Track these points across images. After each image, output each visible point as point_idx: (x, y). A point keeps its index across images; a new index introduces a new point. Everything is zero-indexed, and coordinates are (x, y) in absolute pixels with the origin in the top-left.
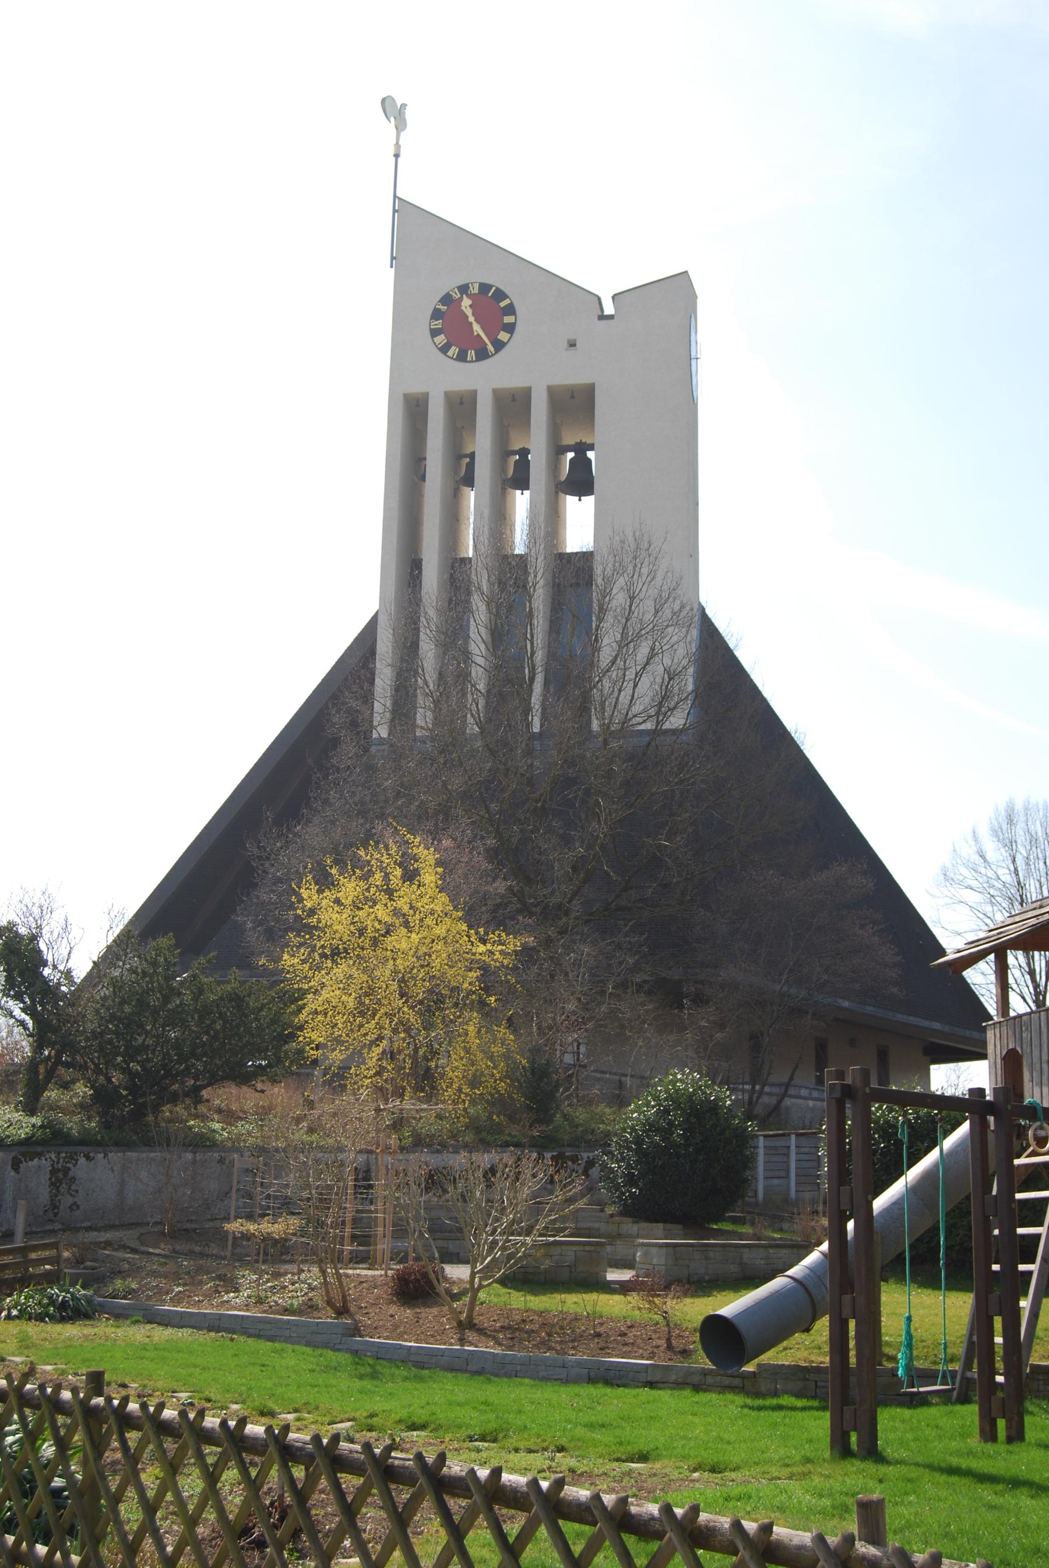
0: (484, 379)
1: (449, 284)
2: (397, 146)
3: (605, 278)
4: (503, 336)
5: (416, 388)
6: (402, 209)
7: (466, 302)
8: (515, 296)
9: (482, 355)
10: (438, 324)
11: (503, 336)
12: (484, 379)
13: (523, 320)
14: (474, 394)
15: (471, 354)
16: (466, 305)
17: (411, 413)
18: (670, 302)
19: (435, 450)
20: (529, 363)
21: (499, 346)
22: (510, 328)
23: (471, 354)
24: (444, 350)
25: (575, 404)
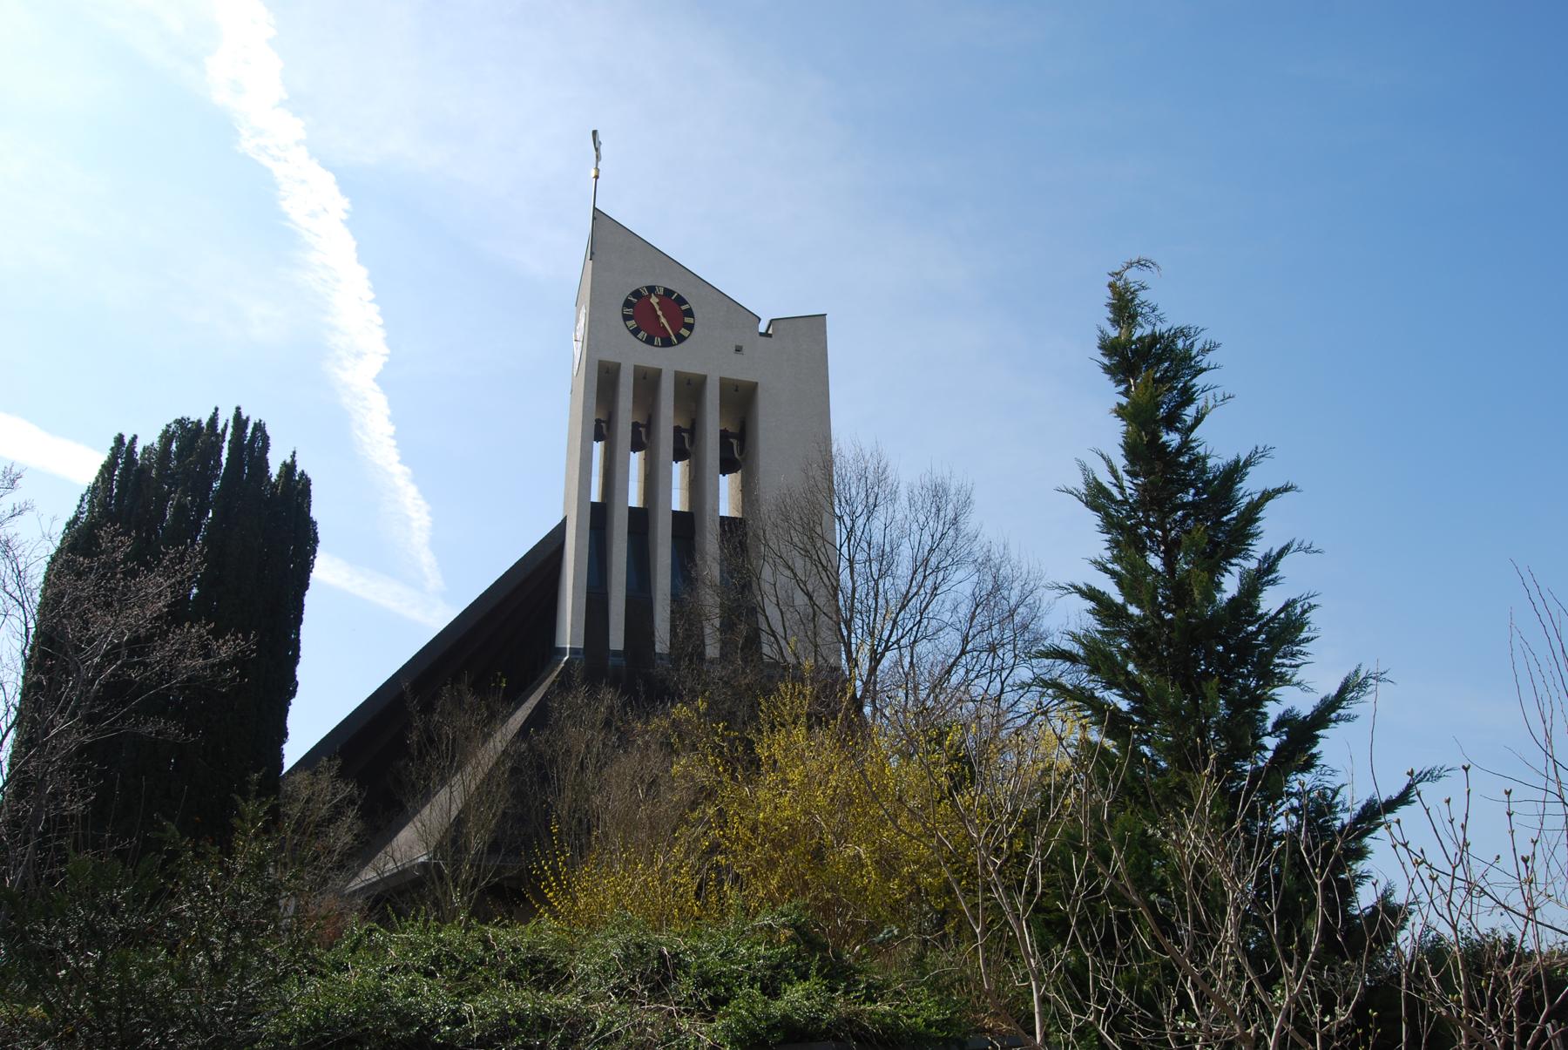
0: (669, 361)
1: (641, 283)
2: (597, 170)
3: (767, 304)
4: (684, 332)
5: (610, 356)
6: (598, 215)
7: (654, 300)
8: (693, 303)
9: (667, 343)
10: (629, 311)
11: (684, 332)
12: (669, 361)
13: (699, 319)
14: (658, 373)
15: (658, 340)
16: (649, 304)
17: (604, 380)
18: (808, 331)
19: (617, 407)
20: (700, 355)
21: (681, 339)
22: (690, 327)
23: (658, 340)
24: (635, 332)
25: (741, 399)
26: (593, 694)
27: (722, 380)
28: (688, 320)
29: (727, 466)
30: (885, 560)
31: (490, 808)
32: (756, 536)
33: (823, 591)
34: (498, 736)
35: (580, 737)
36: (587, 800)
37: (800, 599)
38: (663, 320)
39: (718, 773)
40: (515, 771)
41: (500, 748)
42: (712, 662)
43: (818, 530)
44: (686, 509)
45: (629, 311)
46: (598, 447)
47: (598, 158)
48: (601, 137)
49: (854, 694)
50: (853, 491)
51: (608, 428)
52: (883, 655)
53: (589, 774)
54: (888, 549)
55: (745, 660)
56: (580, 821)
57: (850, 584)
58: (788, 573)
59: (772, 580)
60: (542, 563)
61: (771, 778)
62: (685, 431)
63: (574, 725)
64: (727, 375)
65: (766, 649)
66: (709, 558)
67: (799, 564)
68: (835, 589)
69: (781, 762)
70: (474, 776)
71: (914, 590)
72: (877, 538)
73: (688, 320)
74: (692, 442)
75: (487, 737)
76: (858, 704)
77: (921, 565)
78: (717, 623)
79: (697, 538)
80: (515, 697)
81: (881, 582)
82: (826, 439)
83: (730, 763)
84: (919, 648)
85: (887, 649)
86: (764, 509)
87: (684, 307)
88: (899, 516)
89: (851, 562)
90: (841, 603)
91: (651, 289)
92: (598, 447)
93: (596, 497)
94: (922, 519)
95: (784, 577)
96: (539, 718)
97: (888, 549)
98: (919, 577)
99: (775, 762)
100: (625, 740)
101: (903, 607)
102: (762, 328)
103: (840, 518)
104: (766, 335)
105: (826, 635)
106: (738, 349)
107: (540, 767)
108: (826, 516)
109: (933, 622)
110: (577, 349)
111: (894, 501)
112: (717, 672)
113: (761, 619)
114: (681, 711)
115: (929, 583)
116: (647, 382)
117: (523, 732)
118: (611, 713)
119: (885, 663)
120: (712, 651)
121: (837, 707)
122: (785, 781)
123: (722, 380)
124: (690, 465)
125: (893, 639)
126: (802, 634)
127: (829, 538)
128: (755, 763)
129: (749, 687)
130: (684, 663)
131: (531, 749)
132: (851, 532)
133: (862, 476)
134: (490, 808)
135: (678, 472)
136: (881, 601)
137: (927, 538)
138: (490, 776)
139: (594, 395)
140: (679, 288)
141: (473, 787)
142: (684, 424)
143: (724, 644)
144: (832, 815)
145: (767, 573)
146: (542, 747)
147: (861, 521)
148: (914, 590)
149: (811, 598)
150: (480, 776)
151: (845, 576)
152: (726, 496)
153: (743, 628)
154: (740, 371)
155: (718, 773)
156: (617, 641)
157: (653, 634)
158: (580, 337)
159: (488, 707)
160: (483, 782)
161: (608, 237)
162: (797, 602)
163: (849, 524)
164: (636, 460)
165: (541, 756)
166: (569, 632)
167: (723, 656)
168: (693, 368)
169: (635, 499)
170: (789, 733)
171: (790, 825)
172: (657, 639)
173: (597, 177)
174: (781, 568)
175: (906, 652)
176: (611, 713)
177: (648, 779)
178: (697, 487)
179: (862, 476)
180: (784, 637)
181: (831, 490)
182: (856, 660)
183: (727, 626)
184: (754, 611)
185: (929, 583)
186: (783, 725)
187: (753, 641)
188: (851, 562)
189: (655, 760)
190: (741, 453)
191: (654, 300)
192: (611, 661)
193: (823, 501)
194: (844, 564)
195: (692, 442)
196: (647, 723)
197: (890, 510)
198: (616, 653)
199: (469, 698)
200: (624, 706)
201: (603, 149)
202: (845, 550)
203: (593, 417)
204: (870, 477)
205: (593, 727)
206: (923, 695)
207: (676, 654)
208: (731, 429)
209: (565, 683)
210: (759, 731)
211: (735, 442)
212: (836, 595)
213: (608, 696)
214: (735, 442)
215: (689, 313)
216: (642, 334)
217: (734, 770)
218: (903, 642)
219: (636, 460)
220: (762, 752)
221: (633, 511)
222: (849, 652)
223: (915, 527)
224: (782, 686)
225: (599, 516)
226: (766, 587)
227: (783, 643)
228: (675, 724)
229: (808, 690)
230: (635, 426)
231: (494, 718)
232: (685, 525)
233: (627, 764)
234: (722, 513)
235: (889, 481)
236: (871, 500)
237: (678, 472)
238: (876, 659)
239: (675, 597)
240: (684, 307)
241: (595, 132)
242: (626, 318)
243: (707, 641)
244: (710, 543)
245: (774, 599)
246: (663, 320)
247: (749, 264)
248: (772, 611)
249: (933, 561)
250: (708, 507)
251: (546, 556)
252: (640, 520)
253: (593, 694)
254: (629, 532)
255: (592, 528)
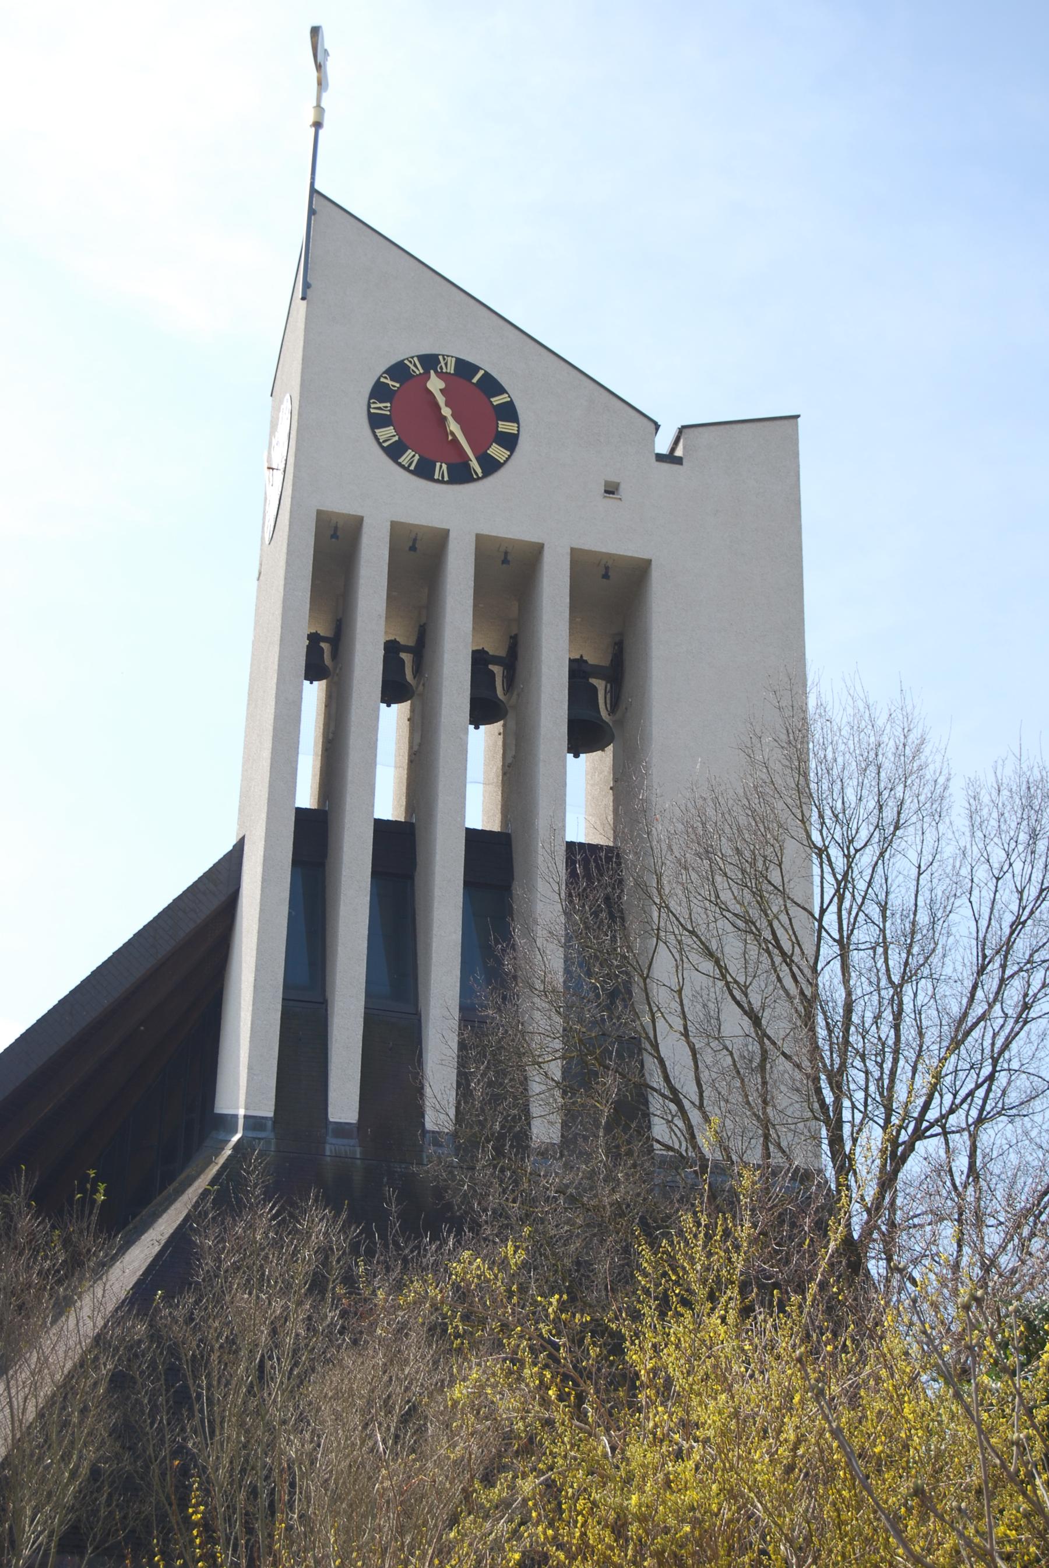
0: (465, 515)
2: (319, 109)
3: (673, 397)
4: (497, 451)
5: (341, 504)
6: (318, 202)
7: (435, 384)
8: (516, 391)
9: (461, 475)
10: (383, 408)
11: (497, 451)
12: (465, 515)
15: (441, 469)
17: (331, 552)
19: (356, 614)
21: (491, 466)
22: (510, 442)
23: (441, 469)
24: (394, 452)
25: (614, 593)
26: (287, 1220)
27: (481, 540)
28: (505, 427)
29: (584, 736)
30: (914, 948)
31: (66, 1458)
32: (641, 886)
33: (783, 1008)
34: (86, 1305)
35: (259, 1308)
36: (271, 1445)
37: (734, 1024)
38: (454, 427)
39: (545, 1402)
40: (119, 1381)
41: (89, 1329)
42: (544, 1153)
43: (775, 876)
44: (495, 827)
45: (383, 408)
46: (313, 694)
47: (321, 84)
48: (328, 41)
49: (850, 1234)
50: (851, 795)
51: (335, 654)
52: (910, 1147)
53: (275, 1392)
54: (923, 918)
55: (615, 1154)
56: (254, 1492)
57: (840, 995)
58: (708, 966)
59: (675, 984)
60: (192, 937)
61: (659, 1417)
62: (496, 660)
63: (247, 1286)
64: (487, 530)
65: (659, 1130)
66: (541, 933)
67: (732, 948)
68: (810, 1003)
69: (680, 1383)
70: (35, 1387)
71: (978, 1010)
72: (900, 897)
73: (505, 427)
74: (510, 682)
75: (63, 1306)
76: (853, 1253)
77: (993, 955)
78: (555, 1070)
79: (517, 890)
80: (124, 1221)
81: (908, 990)
82: (793, 680)
83: (572, 1381)
84: (988, 1136)
85: (919, 1134)
86: (660, 830)
87: (497, 400)
88: (949, 850)
89: (844, 946)
90: (822, 1032)
91: (430, 362)
92: (313, 694)
93: (306, 797)
94: (998, 856)
95: (699, 978)
96: (172, 1268)
97: (923, 918)
98: (991, 982)
99: (669, 1381)
100: (356, 1318)
101: (956, 1044)
102: (662, 444)
103: (822, 852)
104: (670, 458)
105: (788, 1102)
106: (611, 490)
107: (173, 1372)
108: (791, 848)
109: (1022, 1082)
110: (273, 486)
111: (938, 816)
112: (554, 1176)
113: (651, 1063)
114: (468, 1265)
115: (1013, 994)
116: (418, 559)
117: (141, 1295)
118: (325, 1263)
119: (914, 1167)
120: (545, 1128)
121: (811, 1263)
122: (687, 1426)
123: (481, 540)
124: (505, 734)
125: (932, 1115)
126: (736, 1098)
127: (796, 892)
128: (629, 1380)
129: (620, 1210)
130: (484, 1157)
131: (155, 1336)
132: (844, 882)
133: (871, 763)
134: (66, 1458)
135: (481, 747)
136: (908, 1032)
137: (1008, 898)
138: (67, 1389)
139: (306, 584)
140: (487, 361)
141: (31, 1415)
142: (494, 647)
143: (570, 1116)
144: (786, 1501)
145: (663, 966)
146: (178, 1332)
147: (865, 860)
148: (978, 1010)
149: (756, 1021)
150: (47, 1390)
151: (830, 977)
152: (580, 800)
153: (610, 1083)
154: (614, 536)
155: (545, 1402)
156: (344, 1103)
157: (420, 1091)
158: (278, 462)
159: (66, 1242)
160: (51, 1401)
161: (337, 248)
162: (727, 1030)
163: (840, 863)
164: (392, 722)
165: (174, 1351)
166: (245, 1081)
167: (567, 1142)
168: (514, 527)
169: (387, 802)
170: (698, 1324)
171: (696, 1523)
172: (429, 1102)
173: (318, 125)
174: (694, 957)
175: (960, 1142)
176: (325, 1263)
177: (399, 1408)
178: (517, 777)
179: (871, 763)
180: (698, 1102)
181: (803, 792)
182: (850, 1158)
183: (578, 1078)
184: (636, 1046)
185: (1013, 994)
186: (686, 1303)
187: (632, 1111)
188: (844, 946)
189: (417, 1357)
190: (612, 711)
191: (435, 384)
192: (332, 1146)
193: (784, 815)
194: (829, 950)
195: (510, 682)
196: (399, 1287)
197: (930, 837)
198: (342, 1129)
199: (26, 1223)
200: (355, 1248)
201: (331, 67)
202: (830, 919)
203: (303, 629)
204: (888, 765)
205: (287, 1289)
206: (993, 1237)
207: (468, 1136)
208: (592, 658)
209: (227, 1197)
210: (636, 1316)
211: (600, 684)
212: (809, 1021)
213: (319, 1226)
214: (600, 684)
215: (509, 412)
216: (409, 457)
217: (581, 1398)
218: (953, 1120)
219: (392, 722)
220: (639, 1359)
221: (381, 827)
222: (836, 1141)
223: (982, 873)
224: (687, 1220)
225: (312, 838)
226: (662, 997)
227: (695, 1116)
228: (462, 1294)
229: (744, 1232)
230: (392, 649)
231: (79, 1266)
232: (492, 861)
233: (358, 1371)
234: (570, 837)
235: (929, 774)
236: (889, 814)
237: (481, 747)
238: (895, 1156)
239: (469, 1015)
240: (497, 400)
241: (315, 31)
242: (376, 422)
243: (535, 1110)
244: (545, 900)
245: (678, 1023)
246: (454, 427)
247: (630, 302)
248: (672, 1047)
249: (1021, 947)
250: (542, 823)
251: (200, 922)
252: (398, 849)
253: (287, 1220)
254: (375, 874)
255: (297, 862)
